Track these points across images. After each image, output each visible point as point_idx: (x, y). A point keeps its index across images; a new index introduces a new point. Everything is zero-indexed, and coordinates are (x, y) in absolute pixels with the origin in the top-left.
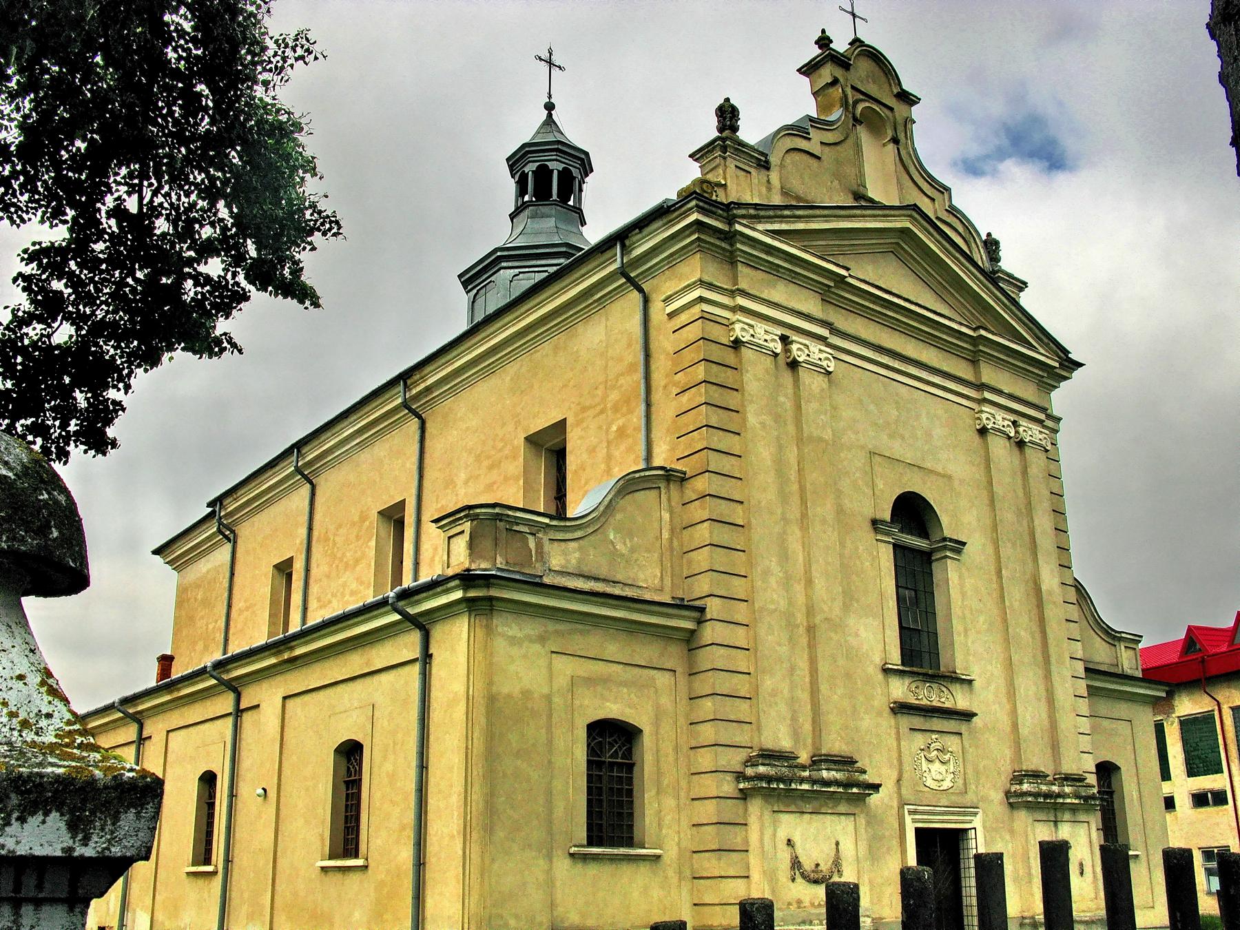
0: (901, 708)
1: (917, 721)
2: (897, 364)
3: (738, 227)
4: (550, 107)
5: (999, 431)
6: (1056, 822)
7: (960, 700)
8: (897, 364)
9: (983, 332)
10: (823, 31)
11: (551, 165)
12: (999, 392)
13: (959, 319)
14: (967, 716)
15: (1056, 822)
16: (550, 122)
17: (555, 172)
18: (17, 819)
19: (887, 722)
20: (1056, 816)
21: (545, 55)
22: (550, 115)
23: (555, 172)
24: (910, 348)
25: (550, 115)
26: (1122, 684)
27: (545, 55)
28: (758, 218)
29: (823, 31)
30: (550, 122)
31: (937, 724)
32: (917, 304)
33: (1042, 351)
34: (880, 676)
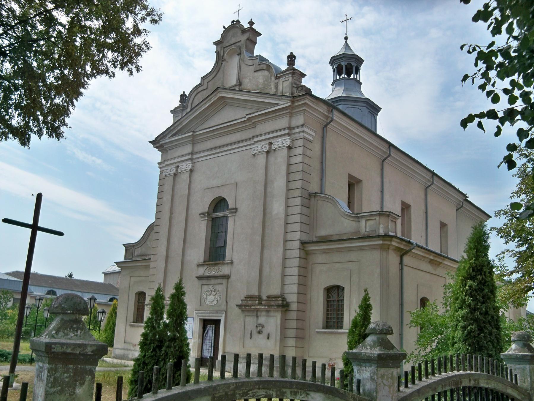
0: (199, 278)
1: (204, 282)
2: (230, 148)
3: (161, 143)
4: (346, 38)
5: (260, 152)
6: (257, 316)
7: (225, 270)
8: (226, 149)
9: (248, 116)
10: (251, 20)
11: (343, 64)
12: (261, 135)
13: (253, 111)
14: (227, 277)
15: (257, 316)
16: (346, 45)
17: (344, 67)
18: (462, 327)
19: (197, 282)
20: (257, 314)
21: (348, 18)
22: (346, 42)
23: (344, 67)
24: (280, 113)
25: (346, 42)
26: (351, 243)
27: (348, 18)
28: (166, 136)
29: (251, 20)
30: (346, 45)
31: (213, 281)
32: (221, 124)
33: (281, 103)
34: (196, 268)
